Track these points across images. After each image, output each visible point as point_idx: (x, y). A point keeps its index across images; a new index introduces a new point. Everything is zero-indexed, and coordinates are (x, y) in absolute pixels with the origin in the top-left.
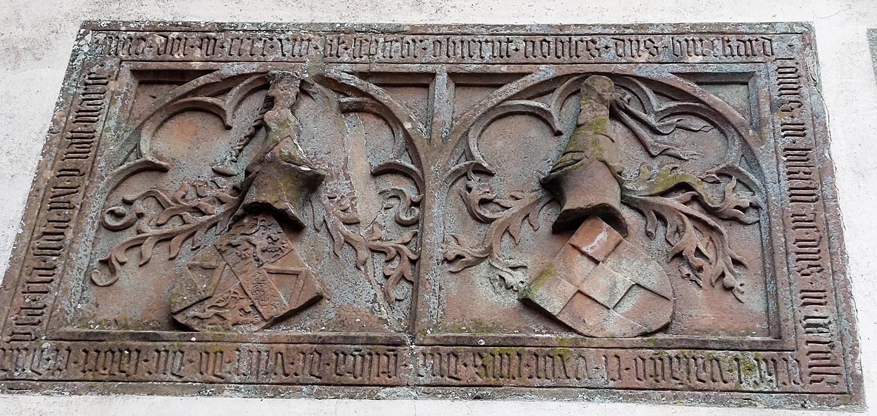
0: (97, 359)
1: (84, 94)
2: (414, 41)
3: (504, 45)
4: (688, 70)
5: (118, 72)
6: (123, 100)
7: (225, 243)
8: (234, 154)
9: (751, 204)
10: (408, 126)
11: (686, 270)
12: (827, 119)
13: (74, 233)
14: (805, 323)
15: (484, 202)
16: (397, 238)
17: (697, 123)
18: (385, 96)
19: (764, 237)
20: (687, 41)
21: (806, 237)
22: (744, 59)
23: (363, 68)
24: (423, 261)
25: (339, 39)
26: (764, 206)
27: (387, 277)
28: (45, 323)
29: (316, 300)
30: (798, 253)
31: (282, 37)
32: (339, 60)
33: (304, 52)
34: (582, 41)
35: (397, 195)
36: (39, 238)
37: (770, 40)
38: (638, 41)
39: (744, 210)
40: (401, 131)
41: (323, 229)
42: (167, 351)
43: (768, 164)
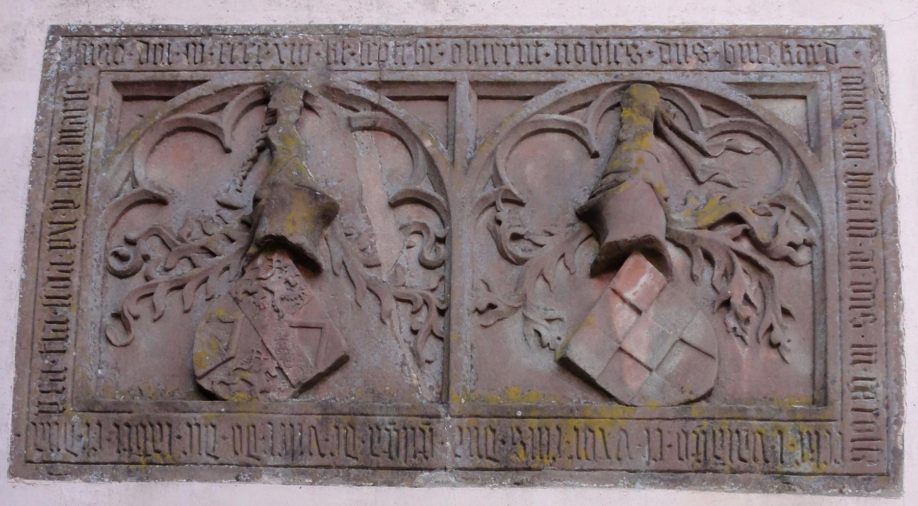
0: (129, 434)
1: (65, 111)
2: (429, 45)
3: (533, 49)
4: (741, 78)
5: (99, 84)
6: (109, 117)
7: (241, 290)
8: (238, 181)
9: (805, 240)
10: (428, 144)
11: (732, 323)
12: (893, 137)
13: (80, 278)
14: (852, 385)
15: (516, 237)
16: (418, 281)
17: (748, 144)
18: (400, 110)
19: (816, 280)
20: (741, 46)
21: (861, 279)
22: (804, 67)
23: (372, 77)
24: (453, 311)
25: (343, 42)
26: (818, 242)
27: (415, 332)
28: (69, 390)
29: (341, 362)
30: (853, 299)
31: (277, 41)
32: (345, 67)
33: (304, 59)
34: (621, 45)
35: (421, 231)
36: (44, 285)
37: (834, 46)
38: (685, 46)
39: (795, 246)
40: (420, 152)
41: (342, 272)
42: (198, 425)
43: (827, 192)
